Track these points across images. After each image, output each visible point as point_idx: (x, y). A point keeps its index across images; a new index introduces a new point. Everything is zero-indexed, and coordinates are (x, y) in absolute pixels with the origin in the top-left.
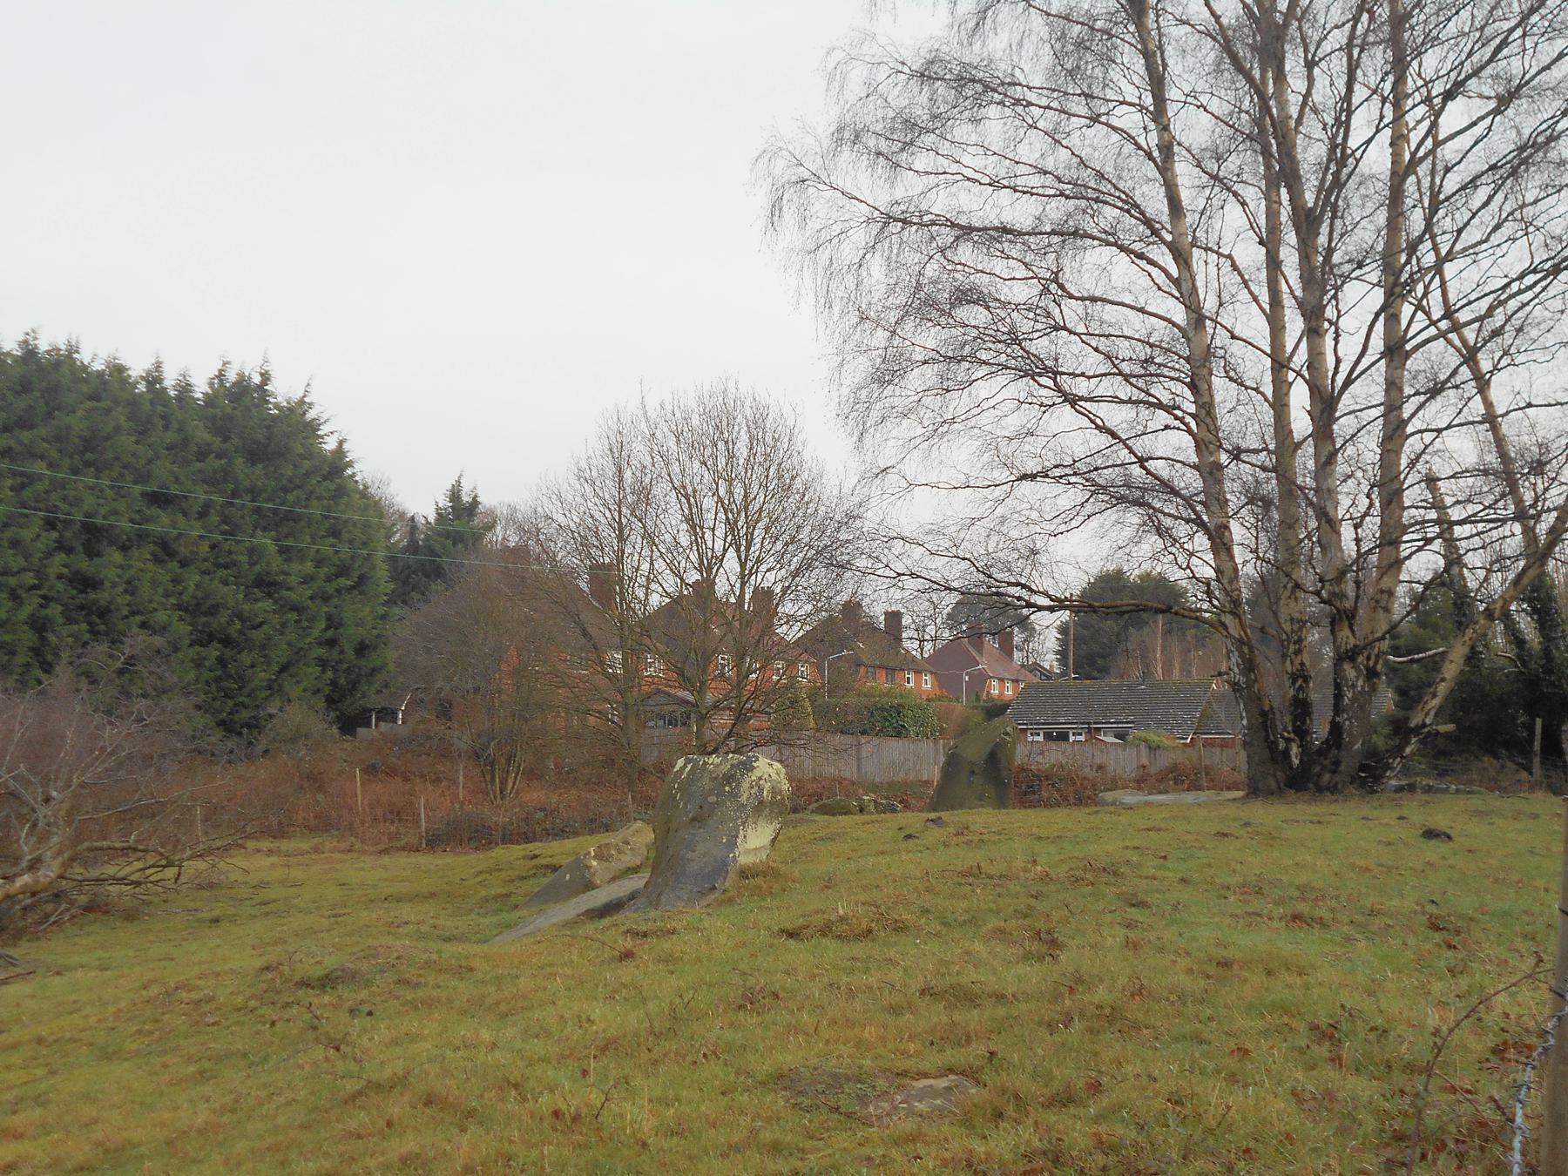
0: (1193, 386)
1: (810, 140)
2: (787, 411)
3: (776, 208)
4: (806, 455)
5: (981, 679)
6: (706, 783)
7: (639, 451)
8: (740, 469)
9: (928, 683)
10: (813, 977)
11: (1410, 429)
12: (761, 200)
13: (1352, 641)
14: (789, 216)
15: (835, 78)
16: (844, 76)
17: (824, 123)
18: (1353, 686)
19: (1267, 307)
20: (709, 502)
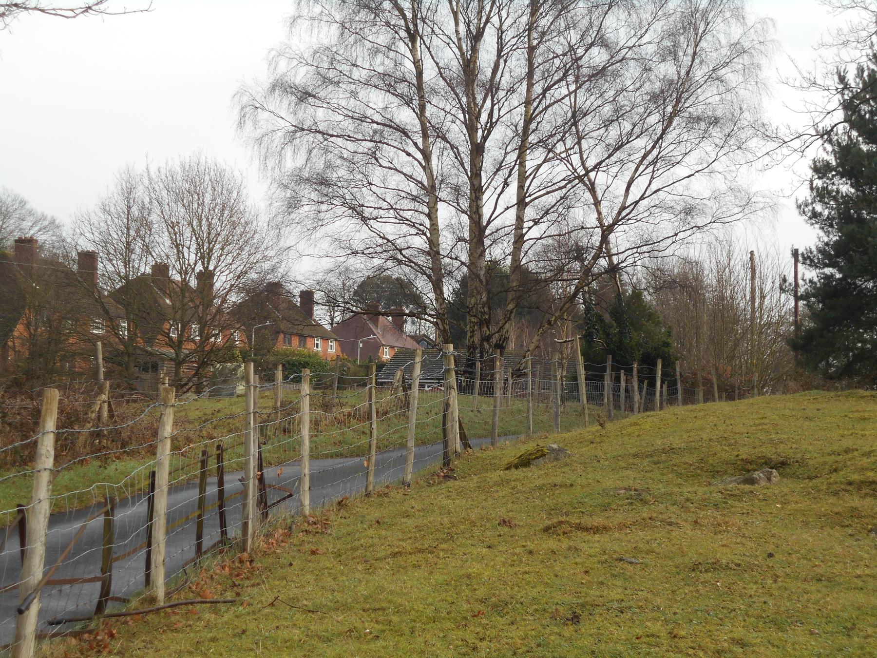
0: (429, 216)
1: (260, 89)
2: (237, 174)
3: (241, 123)
4: (249, 203)
5: (377, 346)
6: (227, 371)
7: (141, 194)
8: (207, 208)
9: (333, 348)
10: (233, 562)
11: (526, 238)
12: (235, 116)
13: (488, 332)
14: (249, 126)
15: (273, 64)
16: (277, 63)
17: (266, 79)
18: (488, 352)
19: (469, 174)
20: (188, 233)
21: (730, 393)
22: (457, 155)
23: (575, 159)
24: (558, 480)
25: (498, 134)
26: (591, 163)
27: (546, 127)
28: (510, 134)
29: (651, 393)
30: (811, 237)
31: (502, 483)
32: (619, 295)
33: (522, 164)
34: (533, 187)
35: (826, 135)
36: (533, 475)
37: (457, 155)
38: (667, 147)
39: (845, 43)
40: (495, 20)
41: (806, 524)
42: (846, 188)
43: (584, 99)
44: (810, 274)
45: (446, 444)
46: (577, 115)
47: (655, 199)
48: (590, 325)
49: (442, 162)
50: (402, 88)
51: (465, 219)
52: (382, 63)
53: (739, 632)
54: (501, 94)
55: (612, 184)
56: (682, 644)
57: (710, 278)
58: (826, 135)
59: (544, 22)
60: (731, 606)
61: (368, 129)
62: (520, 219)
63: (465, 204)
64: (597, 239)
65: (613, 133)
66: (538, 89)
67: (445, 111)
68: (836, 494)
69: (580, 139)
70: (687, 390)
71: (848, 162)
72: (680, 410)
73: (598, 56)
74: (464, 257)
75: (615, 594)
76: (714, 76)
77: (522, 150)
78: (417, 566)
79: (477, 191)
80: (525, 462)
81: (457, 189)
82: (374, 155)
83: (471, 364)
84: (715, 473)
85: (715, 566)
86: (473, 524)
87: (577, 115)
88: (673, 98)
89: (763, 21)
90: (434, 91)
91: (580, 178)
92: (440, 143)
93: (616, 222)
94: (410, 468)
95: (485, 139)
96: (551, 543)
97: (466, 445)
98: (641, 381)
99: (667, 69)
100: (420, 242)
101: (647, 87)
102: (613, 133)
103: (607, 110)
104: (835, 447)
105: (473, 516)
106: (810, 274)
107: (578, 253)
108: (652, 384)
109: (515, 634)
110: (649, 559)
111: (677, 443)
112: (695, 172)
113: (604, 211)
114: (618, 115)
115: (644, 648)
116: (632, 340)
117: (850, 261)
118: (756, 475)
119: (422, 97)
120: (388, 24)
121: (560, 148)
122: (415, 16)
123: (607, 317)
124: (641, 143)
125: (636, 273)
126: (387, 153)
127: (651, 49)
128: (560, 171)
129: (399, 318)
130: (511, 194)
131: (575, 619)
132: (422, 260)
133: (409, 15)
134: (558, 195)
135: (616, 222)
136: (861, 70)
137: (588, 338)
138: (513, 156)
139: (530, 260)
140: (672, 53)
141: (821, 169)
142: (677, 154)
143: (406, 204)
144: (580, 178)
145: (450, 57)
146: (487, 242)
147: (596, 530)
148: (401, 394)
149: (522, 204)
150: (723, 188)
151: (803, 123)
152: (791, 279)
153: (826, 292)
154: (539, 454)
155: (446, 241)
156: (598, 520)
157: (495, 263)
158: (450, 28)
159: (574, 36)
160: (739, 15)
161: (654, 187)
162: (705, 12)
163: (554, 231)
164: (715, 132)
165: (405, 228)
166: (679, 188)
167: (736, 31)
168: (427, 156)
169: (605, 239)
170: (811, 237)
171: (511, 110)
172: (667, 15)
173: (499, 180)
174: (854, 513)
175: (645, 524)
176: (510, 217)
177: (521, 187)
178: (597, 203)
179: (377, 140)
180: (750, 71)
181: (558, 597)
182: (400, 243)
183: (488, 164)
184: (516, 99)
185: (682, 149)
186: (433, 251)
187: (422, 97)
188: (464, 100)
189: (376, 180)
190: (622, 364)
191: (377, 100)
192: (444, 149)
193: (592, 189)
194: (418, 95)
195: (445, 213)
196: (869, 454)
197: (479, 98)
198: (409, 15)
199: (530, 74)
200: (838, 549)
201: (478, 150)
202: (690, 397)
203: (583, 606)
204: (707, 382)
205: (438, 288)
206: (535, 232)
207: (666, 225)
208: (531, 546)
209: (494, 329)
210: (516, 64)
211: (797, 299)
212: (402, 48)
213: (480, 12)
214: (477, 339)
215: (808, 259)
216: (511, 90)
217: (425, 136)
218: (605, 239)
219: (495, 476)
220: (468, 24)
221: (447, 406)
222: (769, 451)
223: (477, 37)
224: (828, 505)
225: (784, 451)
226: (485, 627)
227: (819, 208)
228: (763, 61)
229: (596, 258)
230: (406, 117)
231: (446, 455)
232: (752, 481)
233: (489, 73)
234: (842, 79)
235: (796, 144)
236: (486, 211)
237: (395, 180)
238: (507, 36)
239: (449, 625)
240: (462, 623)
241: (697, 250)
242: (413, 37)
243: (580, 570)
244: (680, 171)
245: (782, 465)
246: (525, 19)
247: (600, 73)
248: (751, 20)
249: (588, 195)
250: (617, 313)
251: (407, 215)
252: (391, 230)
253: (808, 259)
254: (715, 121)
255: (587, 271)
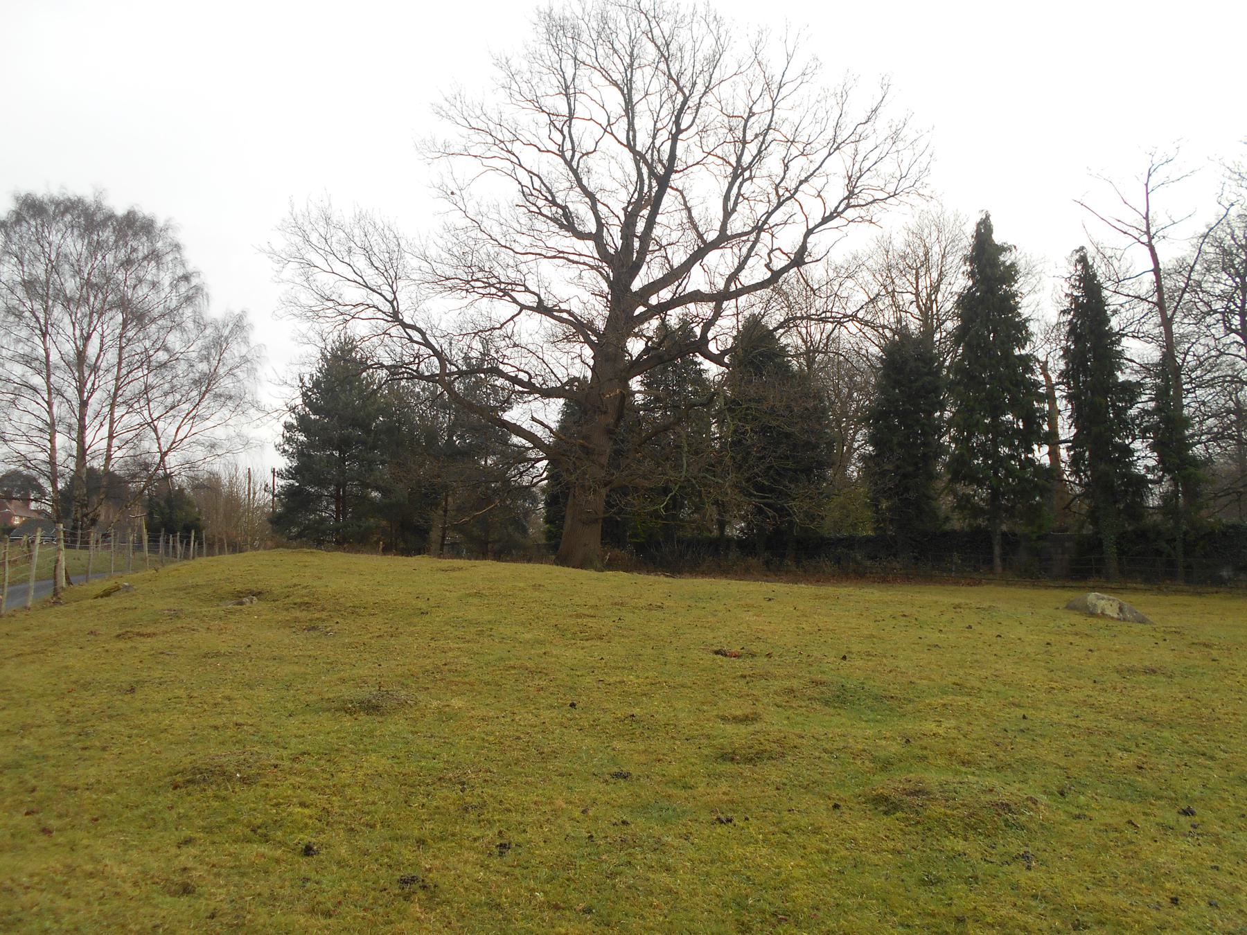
5: (10, 516)
21: (235, 548)
22: (71, 406)
23: (146, 413)
24: (127, 605)
25: (97, 395)
26: (155, 416)
27: (128, 394)
28: (105, 396)
29: (188, 548)
30: (283, 463)
31: (92, 607)
32: (170, 491)
33: (112, 414)
34: (118, 427)
35: (293, 409)
36: (112, 602)
37: (71, 406)
38: (201, 410)
39: (304, 364)
40: (99, 329)
41: (270, 627)
42: (302, 438)
43: (151, 380)
44: (282, 482)
45: (55, 583)
46: (147, 388)
47: (193, 439)
48: (151, 507)
49: (60, 410)
50: (35, 364)
51: (74, 444)
52: (22, 349)
53: (228, 692)
54: (101, 372)
55: (167, 428)
56: (195, 701)
57: (225, 480)
58: (293, 409)
59: (130, 334)
60: (224, 677)
61: (11, 387)
62: (109, 446)
63: (74, 435)
64: (157, 459)
65: (170, 399)
66: (124, 371)
67: (65, 381)
68: (287, 610)
69: (149, 401)
70: (211, 546)
71: (304, 424)
72: (204, 560)
73: (162, 356)
74: (73, 466)
75: (157, 674)
76: (230, 373)
77: (113, 406)
78: (32, 662)
79: (82, 428)
80: (107, 594)
81: (70, 426)
82: (14, 402)
83: (74, 535)
84: (222, 599)
85: (218, 654)
86: (71, 634)
87: (147, 388)
88: (206, 383)
89: (259, 346)
90: (57, 368)
91: (149, 424)
92: (59, 399)
93: (169, 450)
94: (31, 598)
95: (89, 398)
96: (121, 645)
97: (69, 582)
98: (181, 542)
99: (203, 367)
100: (43, 456)
101: (191, 375)
102: (170, 399)
103: (167, 386)
104: (289, 583)
105: (71, 629)
106: (282, 482)
107: (146, 466)
108: (188, 544)
109: (95, 702)
110: (179, 652)
111: (201, 582)
112: (217, 424)
113: (162, 444)
114: (173, 390)
115: (173, 705)
116: (177, 517)
117: (303, 477)
118: (245, 600)
119: (48, 370)
120: (28, 325)
121: (136, 406)
122: (46, 323)
123: (162, 503)
124: (186, 407)
125: (181, 480)
126: (24, 402)
127: (194, 355)
128: (136, 419)
129: (27, 501)
130: (105, 431)
131: (132, 690)
132: (44, 467)
133: (42, 321)
134: (134, 433)
135: (169, 450)
136: (312, 375)
137: (150, 514)
138: (108, 409)
139: (115, 467)
140: (206, 358)
141: (288, 427)
142: (207, 414)
143: (35, 433)
144: (149, 424)
145: (69, 349)
146: (88, 458)
147: (149, 635)
148: (25, 549)
149: (111, 437)
150: (234, 434)
151: (279, 404)
152: (270, 485)
153: (290, 492)
154: (117, 589)
155: (61, 456)
156: (150, 630)
157: (92, 469)
158: (70, 330)
159: (148, 344)
160: (246, 341)
161: (193, 431)
162: (226, 338)
163: (131, 453)
164: (229, 403)
165: (33, 448)
166: (208, 433)
167: (244, 350)
168: (50, 405)
169: (162, 459)
170: (283, 463)
171: (106, 382)
172: (205, 337)
173: (97, 422)
174: (296, 620)
175: (178, 630)
176: (104, 444)
177: (111, 427)
178: (158, 439)
179: (17, 394)
180: (251, 371)
181: (123, 678)
182: (30, 456)
183: (90, 412)
184: (110, 377)
185: (210, 411)
186: (52, 461)
187: (48, 370)
188: (77, 374)
189: (14, 417)
190: (171, 531)
191: (18, 370)
192: (61, 403)
193: (155, 430)
194: (47, 368)
195: (61, 440)
196: (306, 587)
197: (86, 375)
198: (42, 321)
199: (120, 363)
200: (287, 641)
201: (84, 404)
202: (211, 553)
203: (137, 682)
204: (221, 540)
205: (54, 484)
206: (119, 454)
207: (198, 453)
208: (107, 647)
209: (90, 509)
210: (111, 357)
211: (274, 496)
212: (37, 340)
213: (89, 325)
214: (79, 516)
215: (280, 475)
216: (107, 371)
217: (49, 393)
218: (162, 459)
219: (87, 603)
220: (82, 330)
221: (57, 561)
222: (252, 586)
223: (87, 338)
224: (283, 616)
225: (261, 586)
226: (76, 698)
227: (287, 447)
228: (259, 367)
229: (157, 469)
230: (38, 381)
231: (55, 590)
232: (241, 604)
233: (94, 360)
234: (301, 380)
235: (275, 415)
236: (88, 440)
237: (27, 418)
238: (106, 340)
239: (53, 698)
240: (61, 697)
241: (218, 466)
242: (44, 334)
243: (137, 660)
244: (208, 424)
245: (258, 594)
246: (118, 331)
247: (163, 365)
248: (252, 344)
249: (153, 434)
250: (169, 501)
251: (35, 439)
252: (23, 448)
253: (280, 475)
254: (231, 398)
255: (150, 478)
